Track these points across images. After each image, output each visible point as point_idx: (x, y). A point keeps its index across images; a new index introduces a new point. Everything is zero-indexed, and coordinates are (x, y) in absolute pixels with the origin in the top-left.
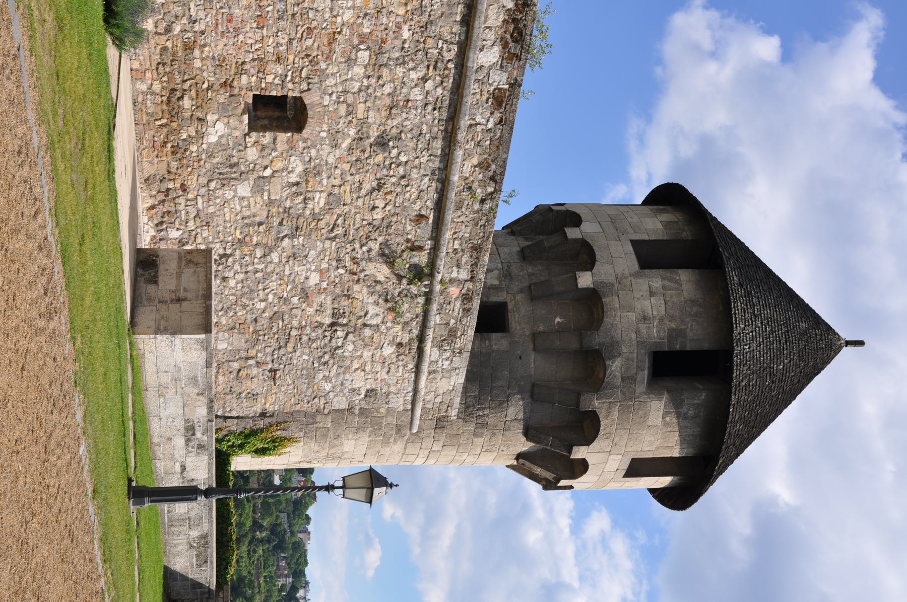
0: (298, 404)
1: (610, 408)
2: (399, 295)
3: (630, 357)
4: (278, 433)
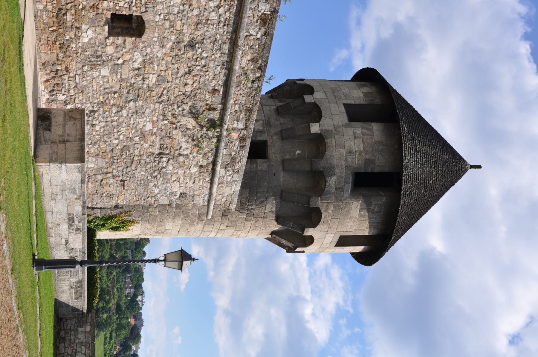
0: (138, 201)
1: (328, 206)
2: (201, 137)
4: (126, 218)
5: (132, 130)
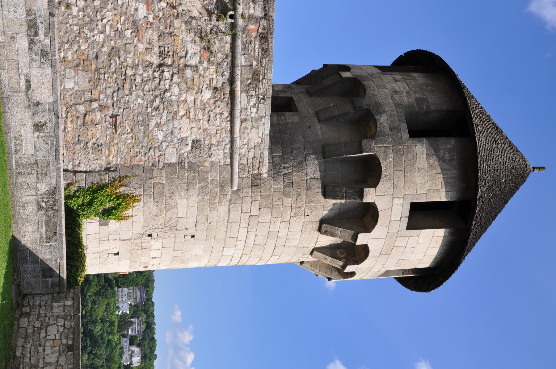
0: (137, 156)
1: (386, 152)
2: (211, 33)
3: (392, 114)
4: (122, 189)
5: (121, 17)
